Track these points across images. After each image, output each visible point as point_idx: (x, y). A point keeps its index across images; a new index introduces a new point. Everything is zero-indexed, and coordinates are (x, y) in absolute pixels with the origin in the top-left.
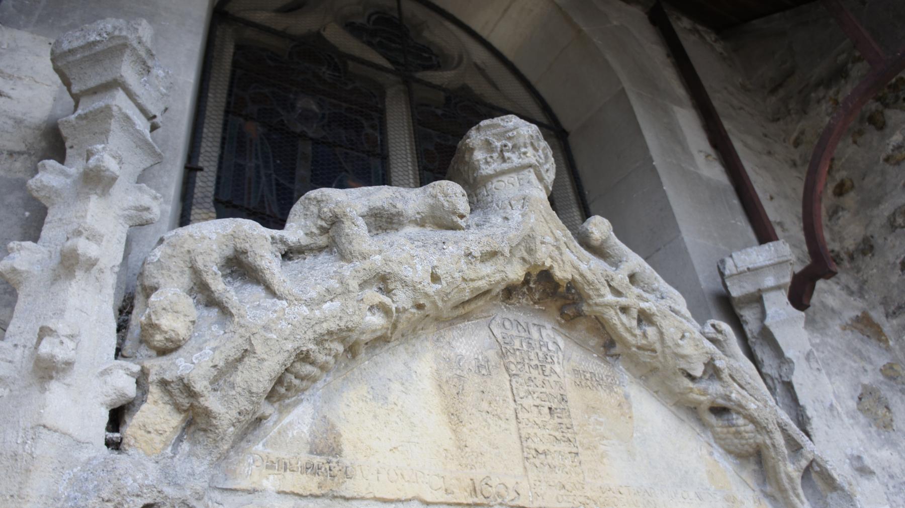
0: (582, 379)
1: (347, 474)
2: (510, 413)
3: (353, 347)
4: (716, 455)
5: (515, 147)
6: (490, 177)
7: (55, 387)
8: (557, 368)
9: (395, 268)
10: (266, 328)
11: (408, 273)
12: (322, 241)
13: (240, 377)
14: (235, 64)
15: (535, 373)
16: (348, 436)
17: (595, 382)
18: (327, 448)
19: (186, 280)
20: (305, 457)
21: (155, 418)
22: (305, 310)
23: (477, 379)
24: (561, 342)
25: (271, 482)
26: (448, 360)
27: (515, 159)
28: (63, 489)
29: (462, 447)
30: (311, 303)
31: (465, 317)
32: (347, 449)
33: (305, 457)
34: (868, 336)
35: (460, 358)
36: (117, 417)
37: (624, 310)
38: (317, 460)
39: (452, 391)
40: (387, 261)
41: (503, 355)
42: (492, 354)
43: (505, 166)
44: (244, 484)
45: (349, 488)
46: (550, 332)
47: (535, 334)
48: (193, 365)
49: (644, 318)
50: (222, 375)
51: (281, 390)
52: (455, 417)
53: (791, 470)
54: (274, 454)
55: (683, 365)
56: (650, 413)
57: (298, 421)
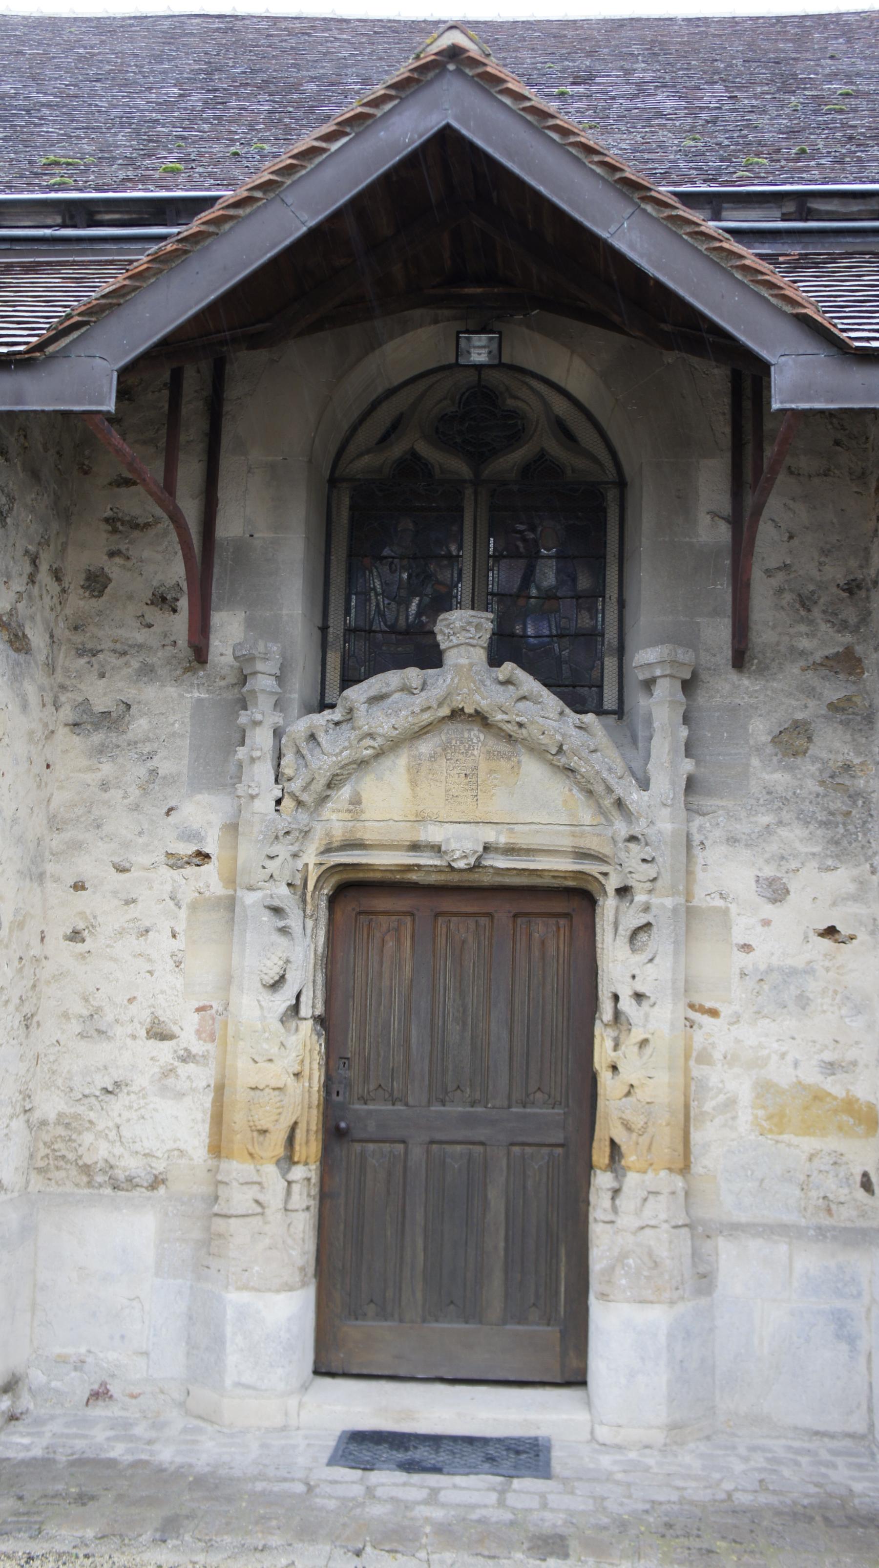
0: (491, 755)
1: (362, 811)
2: (443, 778)
3: (362, 764)
4: (575, 791)
5: (454, 634)
6: (445, 650)
7: (256, 801)
8: (476, 752)
9: (373, 730)
10: (320, 769)
11: (380, 731)
12: (349, 717)
13: (312, 787)
14: (352, 508)
15: (461, 756)
16: (365, 796)
17: (501, 755)
18: (356, 800)
19: (294, 750)
20: (346, 806)
21: (287, 803)
22: (334, 759)
23: (428, 763)
24: (482, 737)
25: (334, 817)
26: (414, 757)
27: (455, 641)
28: (263, 829)
29: (415, 796)
30: (336, 755)
31: (426, 733)
32: (364, 801)
33: (346, 806)
34: (836, 673)
35: (421, 754)
36: (278, 802)
37: (508, 722)
38: (351, 807)
39: (414, 771)
40: (370, 727)
41: (444, 750)
42: (439, 750)
43: (451, 644)
44: (324, 818)
45: (364, 817)
46: (476, 732)
47: (466, 735)
48: (295, 786)
49: (520, 725)
50: (305, 789)
51: (331, 784)
52: (414, 783)
53: (607, 802)
54: (335, 806)
55: (543, 748)
56: (533, 770)
57: (345, 792)
